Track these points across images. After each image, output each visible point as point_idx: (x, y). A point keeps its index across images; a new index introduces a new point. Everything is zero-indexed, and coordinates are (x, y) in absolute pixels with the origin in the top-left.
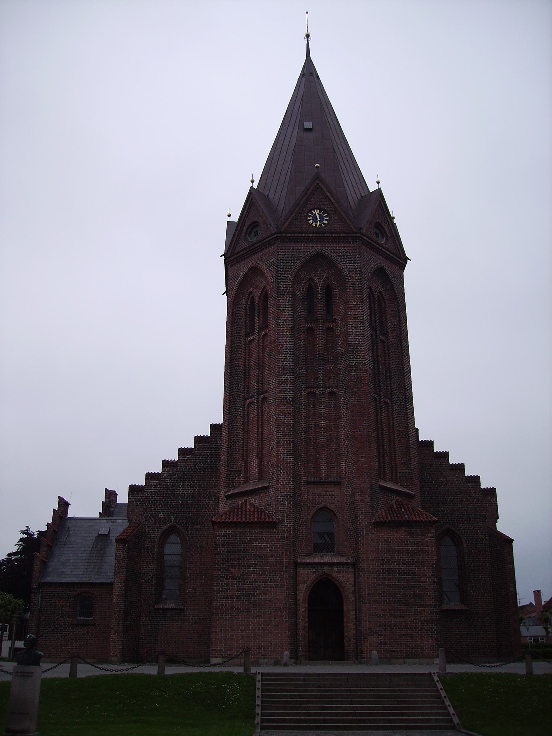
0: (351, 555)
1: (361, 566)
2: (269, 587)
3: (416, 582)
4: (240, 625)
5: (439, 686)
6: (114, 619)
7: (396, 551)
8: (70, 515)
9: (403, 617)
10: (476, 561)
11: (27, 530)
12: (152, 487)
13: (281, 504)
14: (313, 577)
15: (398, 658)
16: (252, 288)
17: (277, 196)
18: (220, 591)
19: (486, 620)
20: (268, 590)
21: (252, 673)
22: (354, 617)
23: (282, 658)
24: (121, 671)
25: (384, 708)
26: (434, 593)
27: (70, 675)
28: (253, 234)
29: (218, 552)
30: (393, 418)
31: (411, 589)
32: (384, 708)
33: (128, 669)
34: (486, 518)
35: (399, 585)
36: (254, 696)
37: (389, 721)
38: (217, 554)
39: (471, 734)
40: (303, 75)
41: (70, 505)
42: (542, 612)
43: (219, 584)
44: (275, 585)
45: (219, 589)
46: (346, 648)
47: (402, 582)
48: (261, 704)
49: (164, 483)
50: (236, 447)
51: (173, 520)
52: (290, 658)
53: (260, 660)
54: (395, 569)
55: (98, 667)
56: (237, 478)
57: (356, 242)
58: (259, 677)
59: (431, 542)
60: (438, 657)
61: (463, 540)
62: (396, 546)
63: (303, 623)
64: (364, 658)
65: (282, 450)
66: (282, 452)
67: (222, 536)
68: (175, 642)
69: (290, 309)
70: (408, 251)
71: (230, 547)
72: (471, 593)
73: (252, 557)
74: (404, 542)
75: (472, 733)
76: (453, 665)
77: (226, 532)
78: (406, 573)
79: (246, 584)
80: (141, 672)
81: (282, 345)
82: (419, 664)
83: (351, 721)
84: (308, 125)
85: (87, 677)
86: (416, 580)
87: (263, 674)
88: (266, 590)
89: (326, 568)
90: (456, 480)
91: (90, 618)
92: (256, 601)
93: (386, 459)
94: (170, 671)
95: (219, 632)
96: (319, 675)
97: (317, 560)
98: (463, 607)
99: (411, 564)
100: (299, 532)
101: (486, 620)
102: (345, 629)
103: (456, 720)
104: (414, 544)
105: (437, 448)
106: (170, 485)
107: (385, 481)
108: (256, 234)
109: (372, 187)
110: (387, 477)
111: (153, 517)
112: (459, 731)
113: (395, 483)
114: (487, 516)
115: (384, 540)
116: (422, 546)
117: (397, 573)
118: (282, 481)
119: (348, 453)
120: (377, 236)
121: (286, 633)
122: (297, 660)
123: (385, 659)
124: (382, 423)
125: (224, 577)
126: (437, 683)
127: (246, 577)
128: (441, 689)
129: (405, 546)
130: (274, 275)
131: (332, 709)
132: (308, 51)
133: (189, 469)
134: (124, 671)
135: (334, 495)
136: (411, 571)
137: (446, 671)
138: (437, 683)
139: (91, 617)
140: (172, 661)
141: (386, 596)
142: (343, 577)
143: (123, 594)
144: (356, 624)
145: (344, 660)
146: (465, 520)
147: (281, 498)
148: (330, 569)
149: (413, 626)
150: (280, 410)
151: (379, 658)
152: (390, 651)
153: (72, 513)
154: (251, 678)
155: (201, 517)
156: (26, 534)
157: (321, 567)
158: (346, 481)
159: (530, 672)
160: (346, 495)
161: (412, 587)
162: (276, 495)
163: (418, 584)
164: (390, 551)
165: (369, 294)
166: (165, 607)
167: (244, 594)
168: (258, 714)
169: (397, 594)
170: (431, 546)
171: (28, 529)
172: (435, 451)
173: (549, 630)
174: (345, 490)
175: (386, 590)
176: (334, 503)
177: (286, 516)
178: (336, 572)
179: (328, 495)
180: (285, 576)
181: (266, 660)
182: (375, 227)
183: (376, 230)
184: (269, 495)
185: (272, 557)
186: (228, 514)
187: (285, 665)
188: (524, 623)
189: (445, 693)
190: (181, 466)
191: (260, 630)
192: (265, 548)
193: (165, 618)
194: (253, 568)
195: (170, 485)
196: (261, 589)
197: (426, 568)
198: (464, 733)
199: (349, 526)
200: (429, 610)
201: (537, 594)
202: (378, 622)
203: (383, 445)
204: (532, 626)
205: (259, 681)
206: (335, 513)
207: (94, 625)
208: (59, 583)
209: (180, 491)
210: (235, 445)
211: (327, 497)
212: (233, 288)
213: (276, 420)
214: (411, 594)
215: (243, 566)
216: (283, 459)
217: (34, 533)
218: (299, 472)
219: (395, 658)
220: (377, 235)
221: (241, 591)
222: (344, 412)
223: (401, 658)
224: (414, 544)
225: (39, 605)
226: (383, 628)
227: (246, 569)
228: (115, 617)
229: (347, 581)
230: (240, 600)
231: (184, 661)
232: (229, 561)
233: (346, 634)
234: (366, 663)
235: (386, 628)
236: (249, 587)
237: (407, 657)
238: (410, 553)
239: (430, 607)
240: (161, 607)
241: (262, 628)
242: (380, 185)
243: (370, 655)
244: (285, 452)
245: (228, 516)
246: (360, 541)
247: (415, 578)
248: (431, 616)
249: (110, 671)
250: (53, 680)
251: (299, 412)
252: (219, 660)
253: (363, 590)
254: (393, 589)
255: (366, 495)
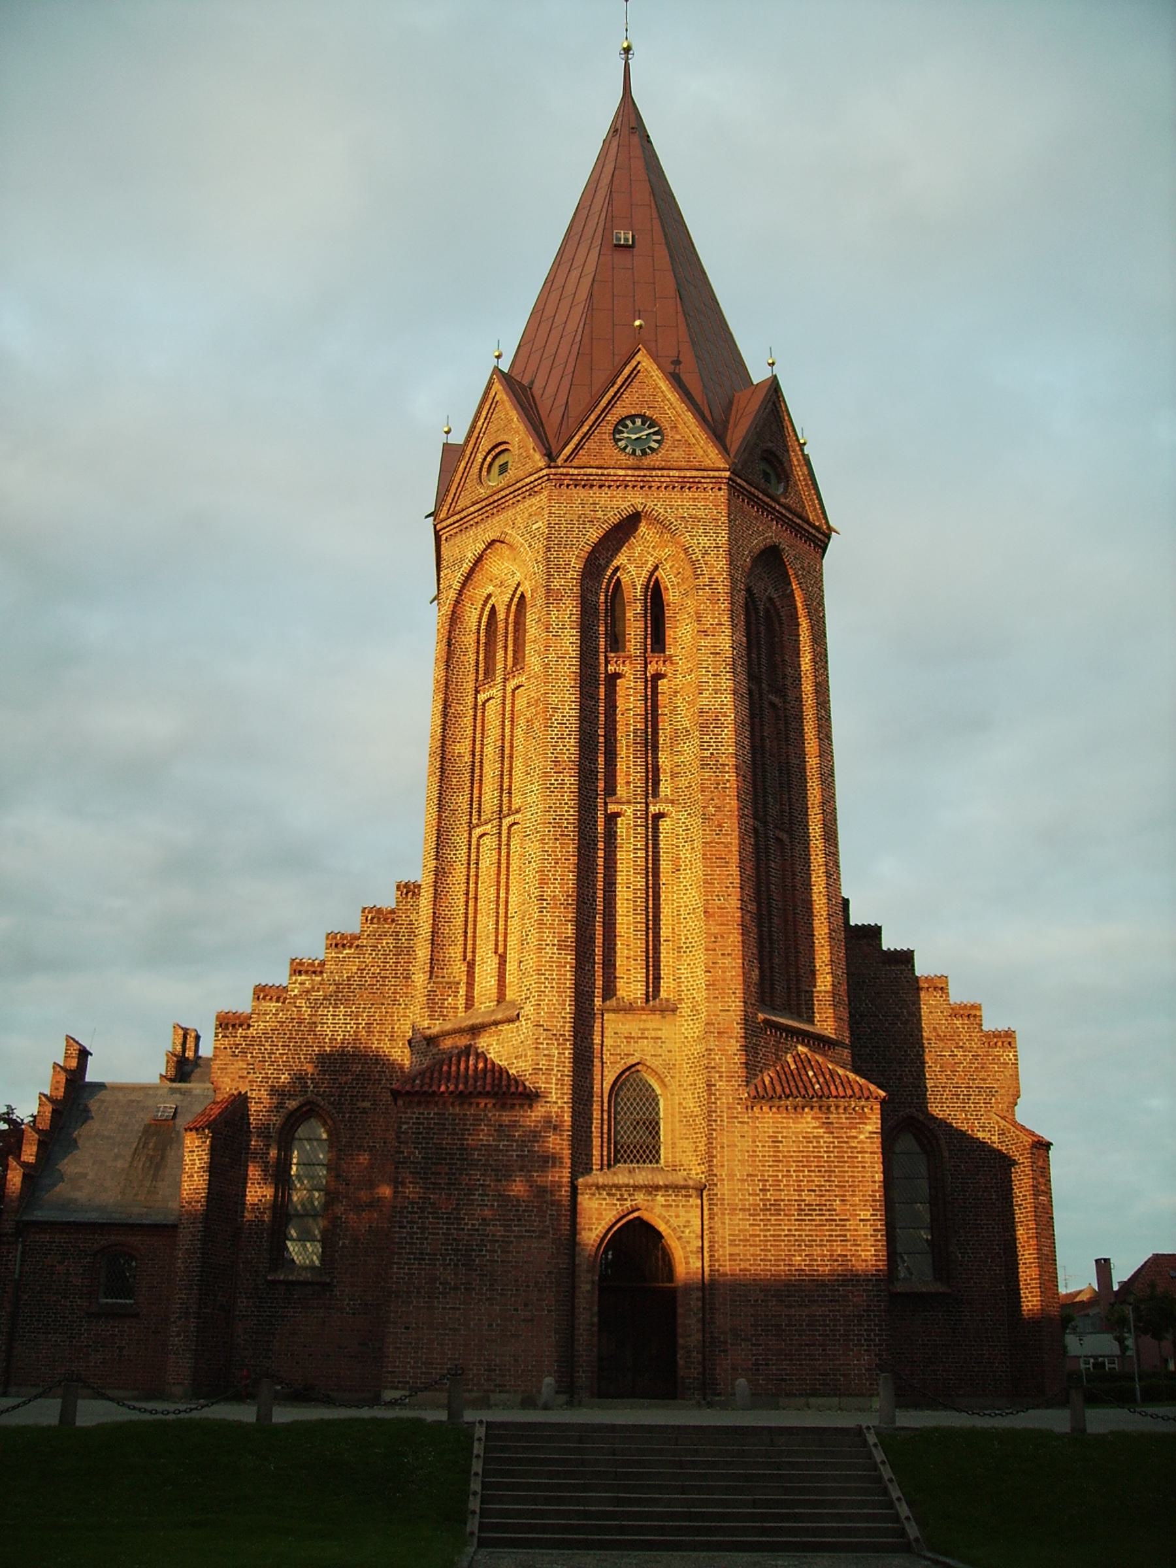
0: (696, 1169)
1: (716, 1194)
2: (515, 1237)
3: (836, 1231)
4: (450, 1318)
5: (879, 1455)
6: (177, 1303)
7: (794, 1161)
8: (88, 1079)
9: (806, 1306)
10: (969, 1187)
11: (8, 1113)
12: (268, 1017)
13: (545, 1055)
14: (610, 1216)
15: (795, 1395)
16: (491, 587)
17: (551, 390)
18: (406, 1243)
19: (988, 1316)
20: (512, 1242)
21: (467, 1423)
22: (700, 1304)
23: (539, 1392)
24: (174, 1413)
25: (755, 1504)
26: (875, 1255)
27: (61, 1421)
28: (495, 469)
29: (404, 1157)
30: (794, 874)
31: (825, 1246)
32: (755, 1504)
33: (191, 1410)
34: (993, 1095)
35: (799, 1236)
36: (466, 1471)
37: (764, 1531)
38: (400, 1162)
39: (944, 1563)
40: (614, 131)
41: (91, 1054)
42: (1112, 1305)
43: (405, 1227)
44: (526, 1231)
45: (405, 1238)
46: (681, 1373)
47: (804, 1230)
48: (483, 1489)
49: (294, 1009)
50: (451, 930)
51: (311, 1088)
52: (557, 1392)
53: (492, 1395)
54: (791, 1200)
55: (134, 1408)
56: (450, 999)
57: (720, 489)
58: (480, 1432)
59: (872, 1143)
60: (878, 1395)
61: (942, 1142)
62: (794, 1152)
63: (587, 1317)
64: (719, 1394)
65: (548, 937)
66: (548, 942)
67: (413, 1123)
68: (310, 1355)
69: (574, 632)
70: (1150, 1255)
71: (431, 1148)
72: (957, 1257)
73: (478, 1170)
74: (811, 1142)
75: (948, 1560)
76: (913, 1413)
77: (423, 1114)
78: (815, 1210)
79: (463, 1229)
80: (218, 1416)
81: (555, 709)
82: (840, 1409)
83: (679, 1530)
84: (624, 236)
85: (100, 1427)
86: (836, 1225)
87: (489, 1425)
88: (507, 1242)
89: (640, 1198)
90: (931, 1012)
91: (127, 1301)
92: (486, 1265)
93: (777, 961)
94: (283, 1415)
95: (402, 1333)
96: (613, 1428)
97: (621, 1179)
98: (942, 1288)
99: (826, 1191)
100: (584, 1118)
101: (988, 1316)
102: (680, 1330)
103: (913, 1531)
104: (834, 1147)
105: (889, 942)
106: (306, 1012)
107: (774, 1009)
108: (504, 469)
109: (758, 374)
110: (778, 1002)
111: (267, 1082)
112: (919, 1555)
113: (794, 1016)
114: (996, 1092)
115: (769, 1137)
116: (852, 1152)
117: (795, 1210)
118: (548, 1004)
119: (693, 947)
120: (768, 480)
121: (550, 1337)
122: (572, 1396)
123: (763, 1398)
124: (768, 884)
125: (416, 1213)
126: (873, 1449)
127: (465, 1214)
128: (883, 1463)
129: (813, 1152)
130: (539, 559)
131: (639, 1502)
132: (628, 88)
133: (349, 979)
134: (172, 1409)
135: (660, 1038)
136: (825, 1205)
137: (894, 1422)
138: (873, 1449)
139: (131, 1299)
140: (300, 1396)
141: (771, 1261)
142: (677, 1216)
143: (199, 1248)
144: (703, 1320)
145: (675, 1398)
146: (947, 1099)
147: (545, 1042)
148: (650, 1198)
149: (828, 1325)
150: (547, 851)
151: (753, 1395)
152: (777, 1380)
153: (92, 1075)
154: (465, 1434)
155: (374, 1084)
156: (7, 1121)
157: (630, 1195)
158: (688, 1007)
159: (1079, 1429)
160: (687, 1037)
161: (827, 1241)
162: (533, 1035)
163: (840, 1236)
164: (780, 1161)
165: (746, 604)
166: (290, 1278)
167: (458, 1250)
168: (474, 1512)
169: (794, 1255)
170: (871, 1153)
171: (10, 1109)
172: (885, 948)
173: (1127, 1343)
174: (686, 1026)
175: (771, 1245)
176: (661, 1055)
177: (554, 1081)
178: (662, 1206)
179: (647, 1038)
180: (549, 1212)
181: (504, 1396)
182: (764, 459)
183: (763, 466)
184: (519, 1035)
185: (522, 1171)
186: (428, 1074)
187: (546, 1407)
188: (1074, 1328)
189: (889, 1470)
190: (331, 973)
191: (493, 1330)
192: (507, 1151)
193: (289, 1303)
194: (479, 1195)
195: (306, 1012)
196: (498, 1241)
197: (860, 1200)
198: (929, 1559)
199: (691, 1105)
200: (864, 1290)
201: (1103, 1266)
202: (752, 1315)
203: (770, 931)
204: (1091, 1333)
205: (479, 1439)
206: (663, 1076)
207: (137, 1316)
208: (62, 1223)
209: (328, 1027)
210: (449, 926)
211: (645, 1041)
212: (450, 587)
213: (537, 872)
214: (825, 1256)
215: (457, 1189)
216: (551, 958)
217: (22, 1120)
218: (585, 986)
219: (787, 1395)
220: (766, 477)
221: (452, 1244)
222: (686, 858)
223: (801, 1395)
224: (834, 1147)
225: (17, 1272)
226: (762, 1330)
227: (465, 1195)
228: (179, 1298)
229: (684, 1226)
230: (449, 1265)
231: (328, 1396)
232: (427, 1179)
233: (681, 1341)
234: (724, 1406)
235: (768, 1330)
236: (469, 1235)
237: (814, 1393)
238: (824, 1166)
239: (866, 1285)
240: (282, 1278)
241: (498, 1325)
242: (776, 370)
243: (733, 1388)
244: (556, 943)
245: (427, 1080)
246: (716, 1138)
247: (835, 1220)
248: (869, 1306)
249: (151, 1412)
250: (21, 1430)
251: (588, 856)
252: (397, 1394)
253: (721, 1246)
254: (785, 1245)
255: (731, 1037)
